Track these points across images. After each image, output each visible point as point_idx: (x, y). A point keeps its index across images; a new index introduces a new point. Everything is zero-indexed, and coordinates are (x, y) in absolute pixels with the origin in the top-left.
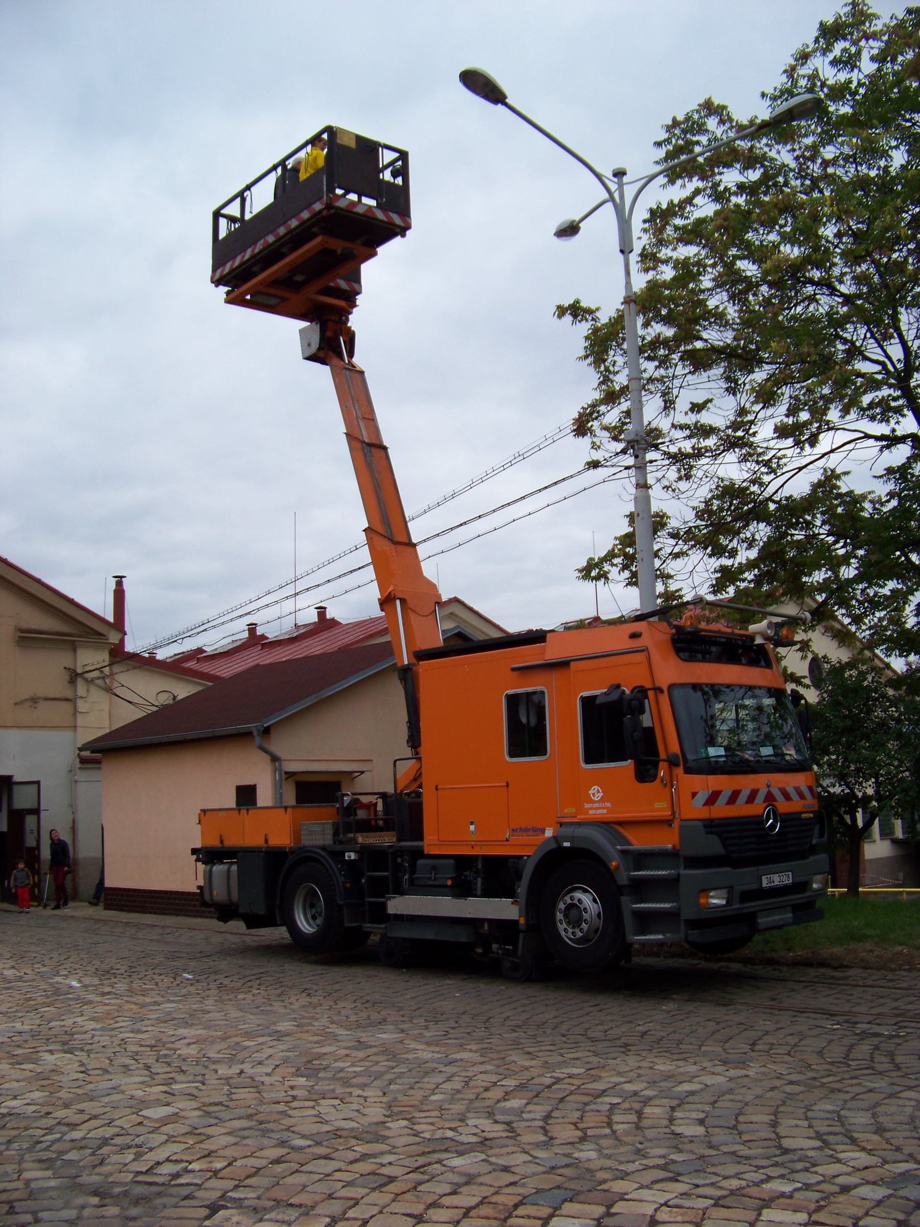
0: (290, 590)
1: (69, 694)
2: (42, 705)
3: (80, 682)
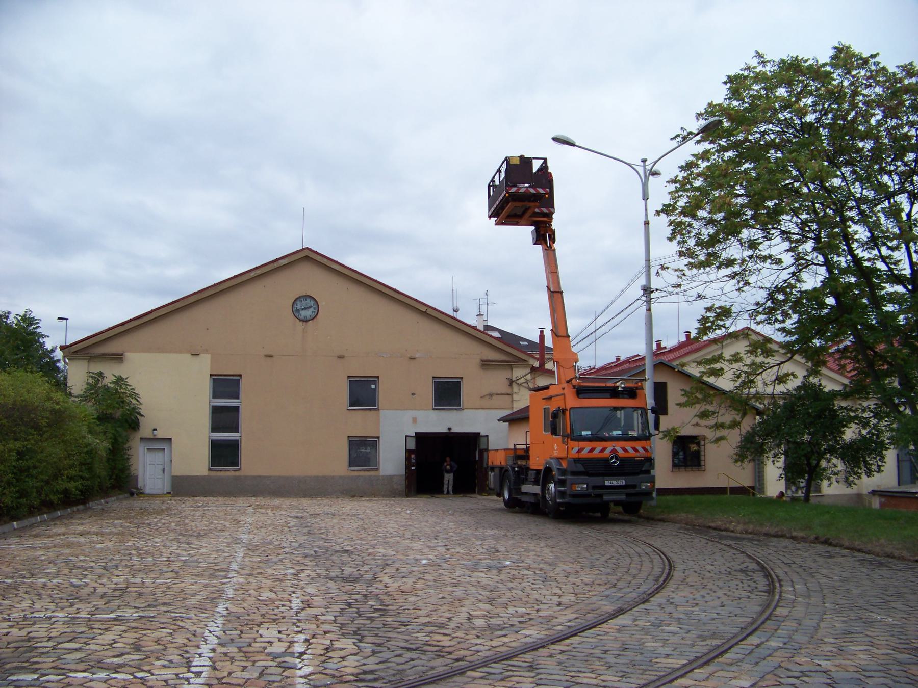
0: (598, 333)
1: (509, 392)
2: (495, 397)
3: (514, 385)
